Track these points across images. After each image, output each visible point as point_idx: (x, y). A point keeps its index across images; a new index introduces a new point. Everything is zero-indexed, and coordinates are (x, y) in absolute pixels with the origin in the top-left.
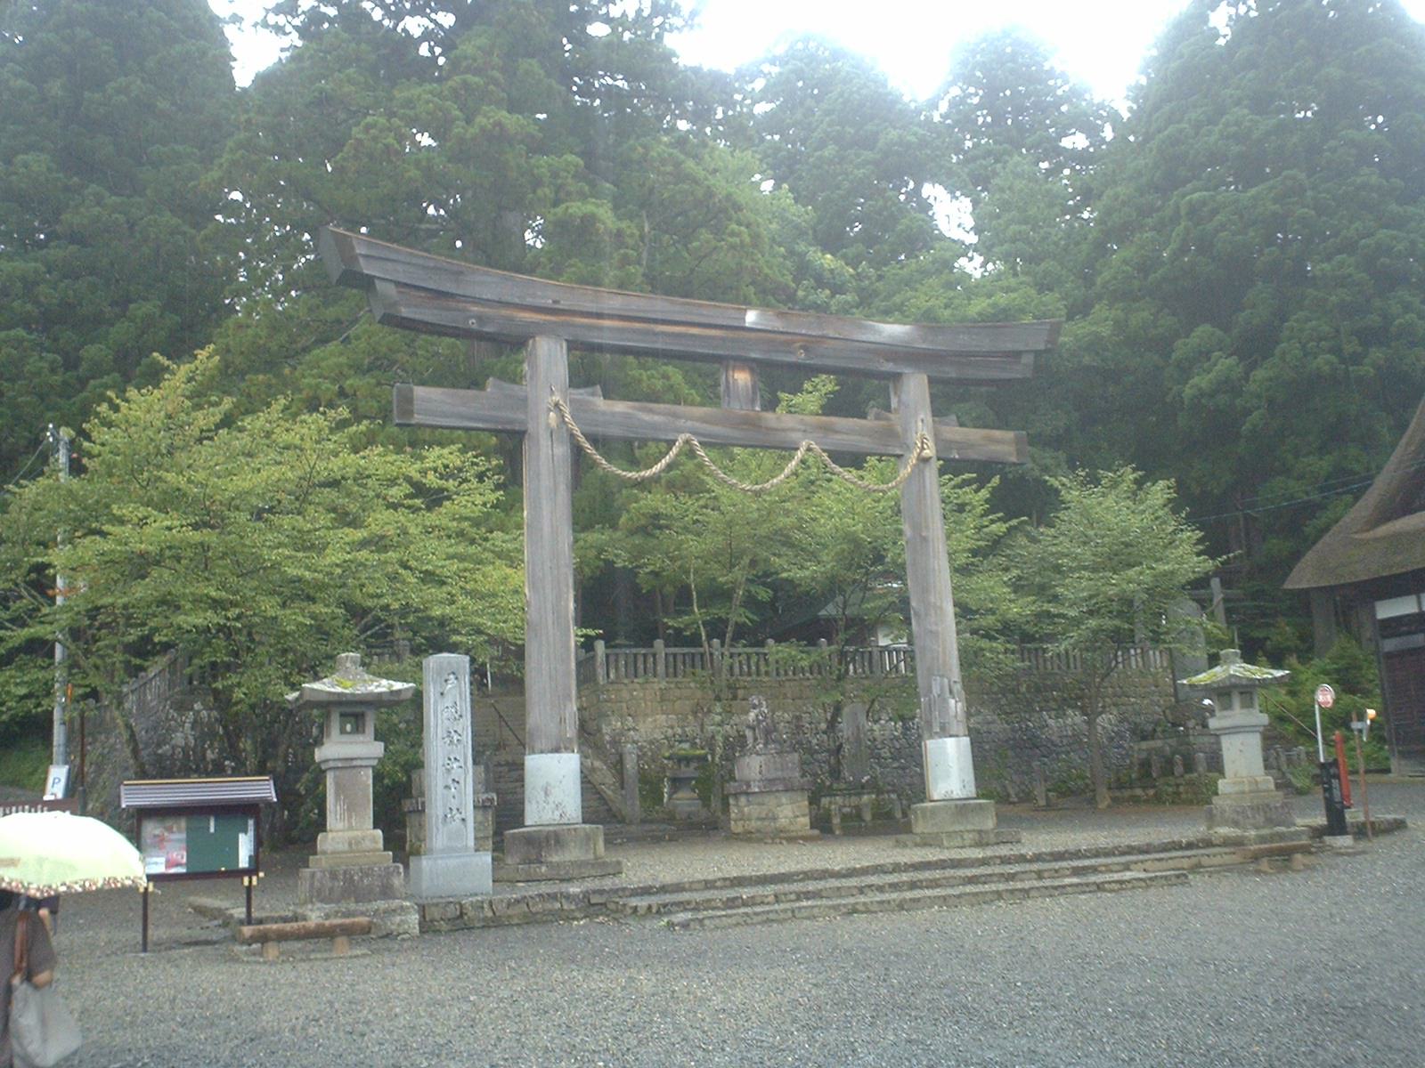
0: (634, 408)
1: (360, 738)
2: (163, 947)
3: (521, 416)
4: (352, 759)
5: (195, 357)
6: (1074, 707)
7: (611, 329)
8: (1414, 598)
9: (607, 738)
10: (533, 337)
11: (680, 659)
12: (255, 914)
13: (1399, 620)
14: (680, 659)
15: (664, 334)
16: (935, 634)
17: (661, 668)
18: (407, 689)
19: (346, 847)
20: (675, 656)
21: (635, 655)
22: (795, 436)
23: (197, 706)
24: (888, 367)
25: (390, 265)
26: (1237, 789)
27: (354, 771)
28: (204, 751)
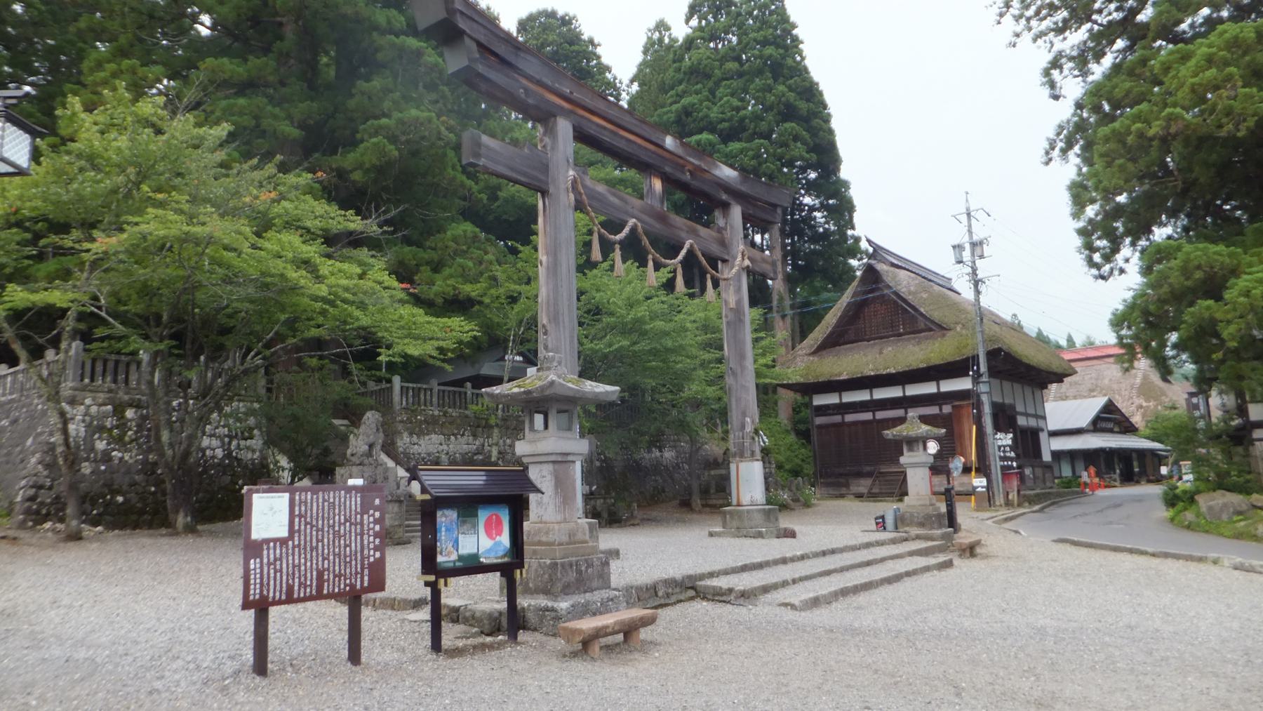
0: (609, 192)
1: (568, 434)
2: (456, 652)
3: (542, 177)
4: (567, 454)
5: (246, 60)
6: (656, 447)
7: (598, 125)
8: (868, 391)
9: (401, 449)
10: (555, 116)
11: (446, 394)
12: (342, 611)
13: (827, 407)
14: (446, 394)
15: (622, 137)
16: (743, 386)
17: (435, 400)
18: (613, 392)
19: (565, 539)
20: (444, 391)
21: (420, 389)
22: (683, 235)
23: (88, 401)
24: (724, 197)
25: (475, 26)
26: (920, 503)
27: (566, 465)
28: (93, 442)
